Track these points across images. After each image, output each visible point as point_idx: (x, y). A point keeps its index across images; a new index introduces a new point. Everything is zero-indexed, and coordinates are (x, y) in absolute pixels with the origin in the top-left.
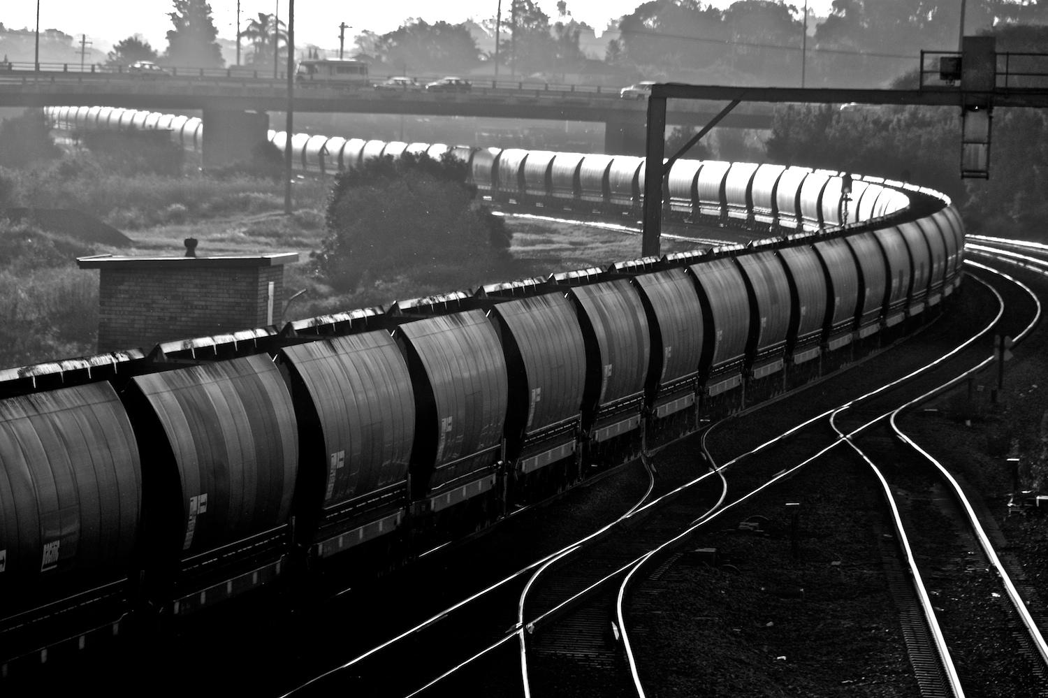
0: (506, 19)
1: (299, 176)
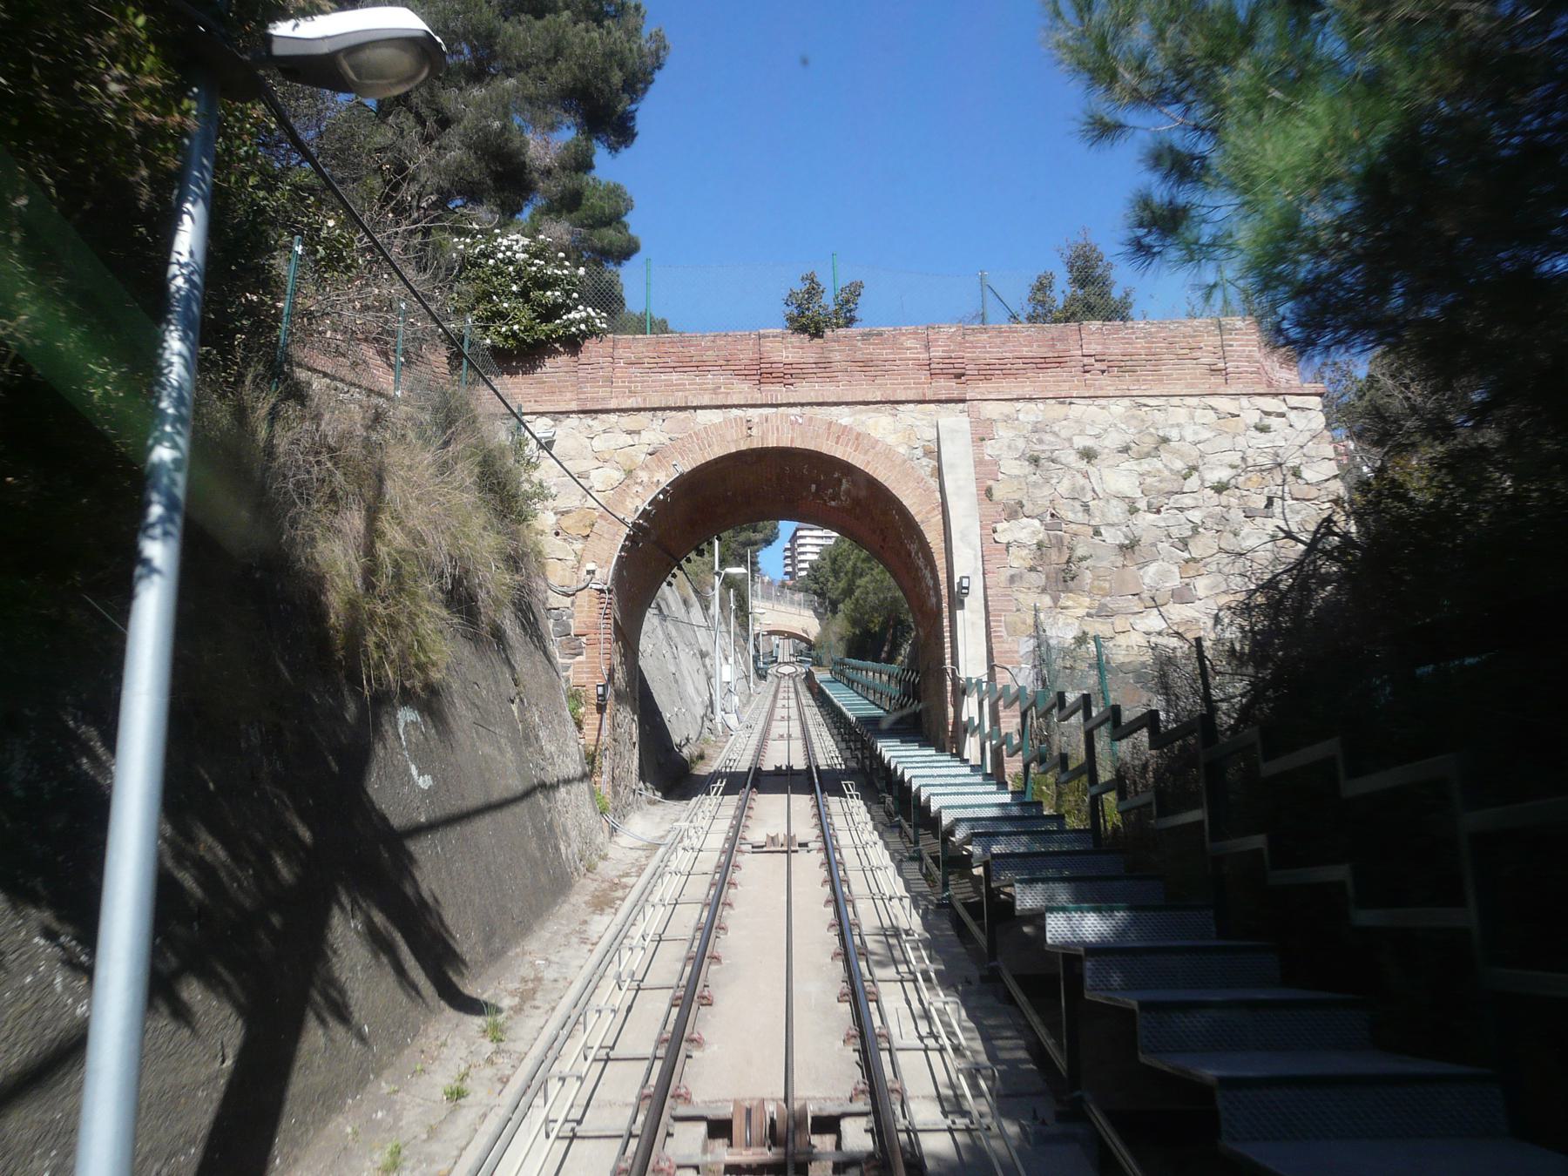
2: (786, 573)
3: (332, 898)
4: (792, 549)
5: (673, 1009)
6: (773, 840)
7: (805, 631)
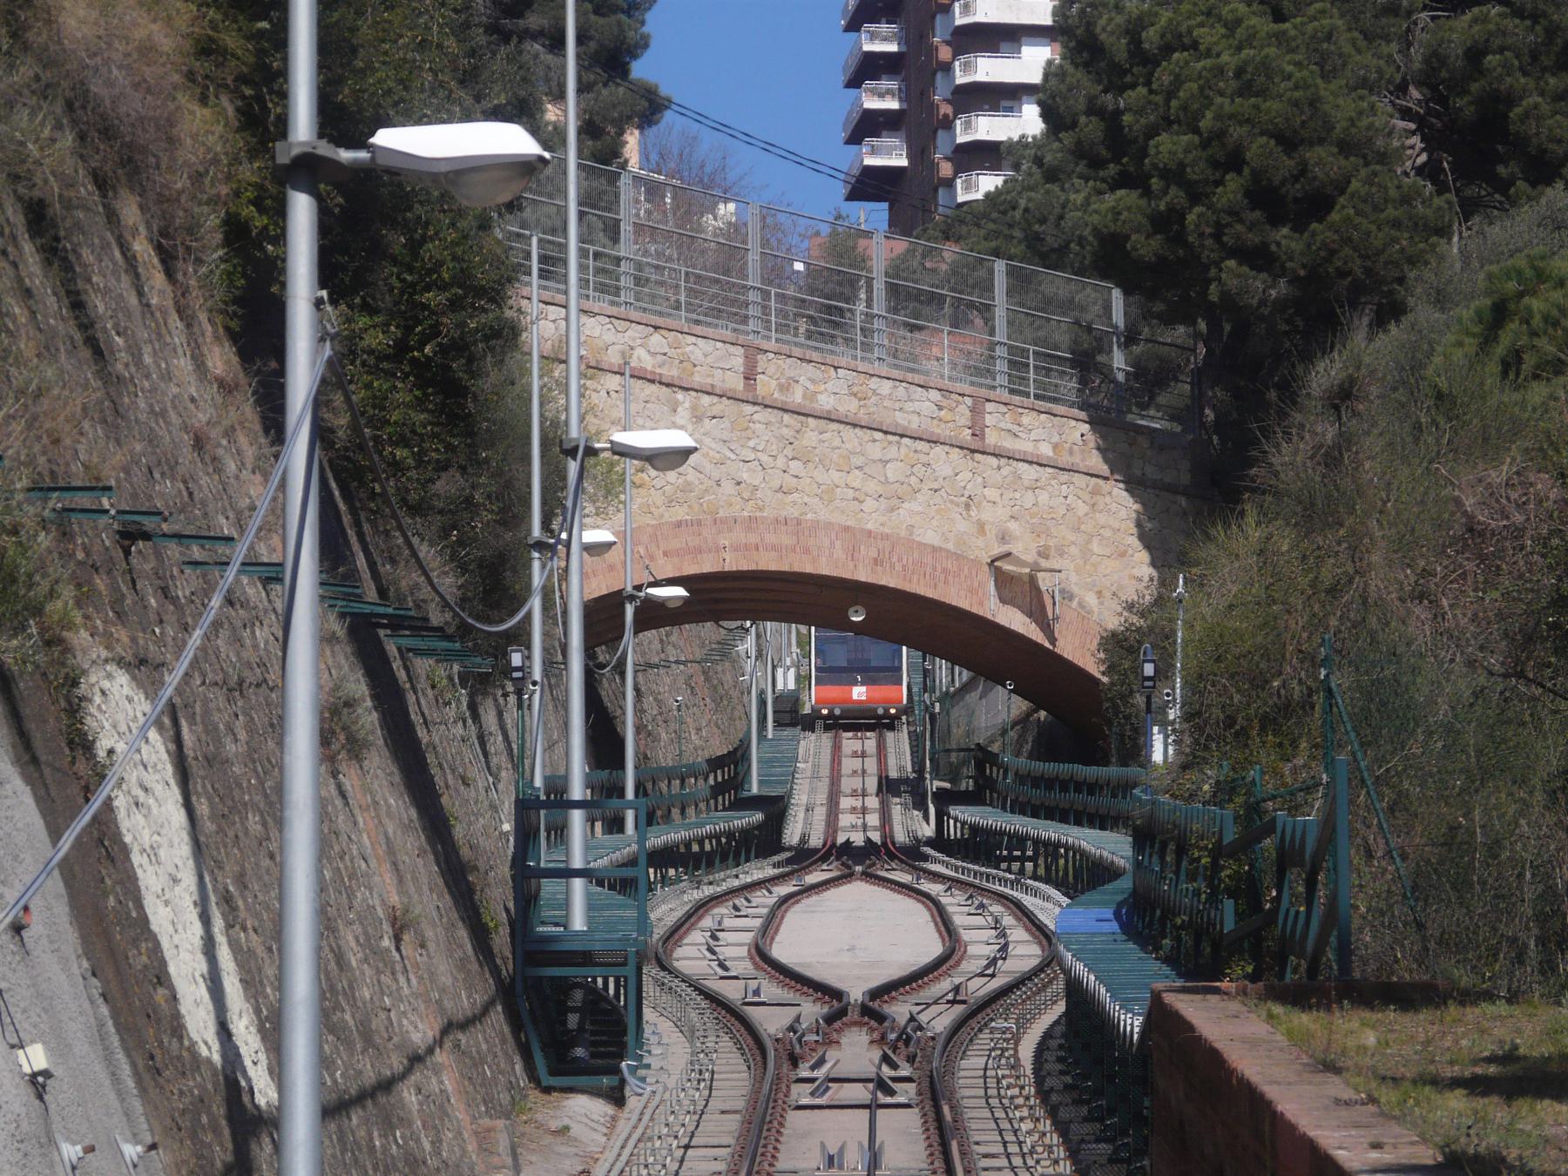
0: (195, 904)
1: (679, 591)
2: (870, 185)
5: (992, 438)
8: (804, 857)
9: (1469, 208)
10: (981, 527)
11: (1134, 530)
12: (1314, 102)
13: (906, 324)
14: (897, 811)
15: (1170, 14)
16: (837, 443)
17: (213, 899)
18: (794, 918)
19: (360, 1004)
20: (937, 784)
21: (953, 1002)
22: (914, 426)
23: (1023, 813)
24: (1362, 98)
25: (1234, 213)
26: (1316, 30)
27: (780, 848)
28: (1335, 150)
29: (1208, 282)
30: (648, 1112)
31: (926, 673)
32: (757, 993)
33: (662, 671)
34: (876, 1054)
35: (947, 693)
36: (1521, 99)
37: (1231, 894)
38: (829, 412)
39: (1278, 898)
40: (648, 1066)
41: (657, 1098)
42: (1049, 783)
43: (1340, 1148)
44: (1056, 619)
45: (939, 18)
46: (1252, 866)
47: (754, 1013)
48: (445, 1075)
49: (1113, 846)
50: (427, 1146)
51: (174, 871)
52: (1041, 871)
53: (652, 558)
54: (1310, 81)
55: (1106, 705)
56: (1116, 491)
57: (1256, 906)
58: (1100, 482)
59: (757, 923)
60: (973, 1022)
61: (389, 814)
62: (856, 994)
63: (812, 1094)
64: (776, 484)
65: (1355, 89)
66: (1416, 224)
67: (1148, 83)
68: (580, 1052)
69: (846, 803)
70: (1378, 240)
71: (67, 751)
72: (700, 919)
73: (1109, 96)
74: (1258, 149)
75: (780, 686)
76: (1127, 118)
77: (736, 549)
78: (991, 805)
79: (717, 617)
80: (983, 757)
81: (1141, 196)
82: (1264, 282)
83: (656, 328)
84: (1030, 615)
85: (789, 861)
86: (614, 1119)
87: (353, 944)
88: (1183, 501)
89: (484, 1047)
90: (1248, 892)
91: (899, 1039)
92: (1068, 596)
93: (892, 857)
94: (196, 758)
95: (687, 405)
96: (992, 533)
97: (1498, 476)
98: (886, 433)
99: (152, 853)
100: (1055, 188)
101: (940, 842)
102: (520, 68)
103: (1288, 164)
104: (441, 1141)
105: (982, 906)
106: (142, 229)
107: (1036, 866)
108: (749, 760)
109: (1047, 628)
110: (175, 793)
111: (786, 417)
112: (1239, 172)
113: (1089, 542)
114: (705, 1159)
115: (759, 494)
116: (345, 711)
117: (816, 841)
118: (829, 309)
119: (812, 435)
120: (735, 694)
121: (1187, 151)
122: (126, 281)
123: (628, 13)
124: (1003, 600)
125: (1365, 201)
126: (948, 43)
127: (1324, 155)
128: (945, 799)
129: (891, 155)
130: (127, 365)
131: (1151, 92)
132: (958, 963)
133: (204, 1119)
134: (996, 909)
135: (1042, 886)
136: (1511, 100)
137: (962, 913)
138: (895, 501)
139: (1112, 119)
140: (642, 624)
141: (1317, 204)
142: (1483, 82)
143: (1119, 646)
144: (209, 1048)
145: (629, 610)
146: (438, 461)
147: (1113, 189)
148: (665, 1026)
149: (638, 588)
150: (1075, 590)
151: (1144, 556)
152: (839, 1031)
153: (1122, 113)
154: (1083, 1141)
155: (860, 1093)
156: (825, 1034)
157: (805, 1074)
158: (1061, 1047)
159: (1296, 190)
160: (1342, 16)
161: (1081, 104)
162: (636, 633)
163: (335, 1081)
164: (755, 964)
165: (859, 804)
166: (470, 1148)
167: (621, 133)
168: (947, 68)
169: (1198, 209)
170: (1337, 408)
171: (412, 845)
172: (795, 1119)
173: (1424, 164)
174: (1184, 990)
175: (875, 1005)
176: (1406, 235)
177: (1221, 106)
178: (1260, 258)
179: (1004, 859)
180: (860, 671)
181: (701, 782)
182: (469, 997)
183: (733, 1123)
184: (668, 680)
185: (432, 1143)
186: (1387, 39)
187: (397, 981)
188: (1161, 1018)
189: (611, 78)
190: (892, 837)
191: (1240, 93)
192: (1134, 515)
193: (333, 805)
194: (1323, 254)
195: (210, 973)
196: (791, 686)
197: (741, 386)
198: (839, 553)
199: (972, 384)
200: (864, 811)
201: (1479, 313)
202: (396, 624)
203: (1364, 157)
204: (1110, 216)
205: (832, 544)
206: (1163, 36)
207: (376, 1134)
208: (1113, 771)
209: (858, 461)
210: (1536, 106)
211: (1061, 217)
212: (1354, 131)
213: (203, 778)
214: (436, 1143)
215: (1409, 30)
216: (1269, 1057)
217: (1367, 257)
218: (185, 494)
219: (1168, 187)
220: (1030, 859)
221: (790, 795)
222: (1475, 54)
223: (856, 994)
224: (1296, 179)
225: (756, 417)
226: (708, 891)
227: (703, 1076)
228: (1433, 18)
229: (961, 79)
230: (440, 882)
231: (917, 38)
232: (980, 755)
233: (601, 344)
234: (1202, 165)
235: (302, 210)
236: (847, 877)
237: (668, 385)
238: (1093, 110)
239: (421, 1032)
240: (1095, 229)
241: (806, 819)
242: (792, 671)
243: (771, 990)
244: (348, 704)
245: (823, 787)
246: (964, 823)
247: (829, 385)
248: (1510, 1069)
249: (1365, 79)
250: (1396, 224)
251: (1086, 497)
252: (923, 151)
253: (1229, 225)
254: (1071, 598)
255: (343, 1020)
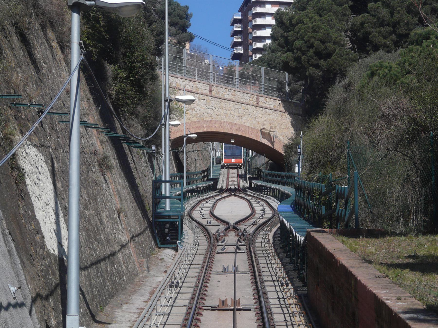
0: (54, 210)
1: (195, 135)
2: (236, 57)
3: (270, 159)
4: (244, 21)
5: (261, 104)
6: (223, 303)
7: (267, 135)
8: (222, 191)
9: (360, 57)
10: (258, 122)
11: (291, 123)
12: (328, 34)
13: (243, 83)
14: (241, 181)
15: (298, 16)
16: (229, 105)
17: (60, 208)
18: (219, 204)
19: (106, 233)
20: (249, 176)
21: (254, 225)
22: (245, 101)
23: (267, 182)
24: (338, 33)
25: (312, 57)
26: (328, 19)
27: (217, 189)
28: (332, 44)
29: (306, 72)
30: (183, 254)
31: (247, 153)
32: (210, 223)
33: (192, 152)
34: (236, 238)
35: (251, 157)
36: (372, 33)
37: (324, 204)
38: (227, 98)
39: (336, 206)
40: (184, 242)
41: (185, 250)
42: (272, 176)
43: (387, 299)
44: (274, 142)
45: (249, 23)
46: (329, 198)
47: (209, 228)
48: (131, 249)
49: (288, 190)
50: (124, 268)
51: (47, 202)
52: (271, 194)
53: (190, 129)
54: (328, 29)
55: (284, 159)
56: (287, 115)
57: (330, 208)
58: (283, 113)
59: (211, 205)
60: (258, 230)
61: (119, 184)
62: (232, 223)
63: (221, 250)
64: (216, 113)
65: (337, 31)
66: (350, 59)
67: (293, 30)
68: (168, 238)
69: (230, 180)
70: (342, 62)
71: (10, 169)
72: (199, 205)
73: (285, 33)
74: (317, 43)
75: (217, 156)
76: (289, 38)
77: (207, 127)
78: (260, 180)
79: (204, 141)
80: (259, 170)
81: (292, 54)
82: (318, 71)
83: (191, 81)
84: (269, 141)
85: (218, 192)
86: (175, 255)
87: (105, 217)
88: (300, 117)
89: (143, 240)
90: (328, 204)
91: (242, 235)
92: (276, 137)
93: (240, 191)
94: (58, 171)
95: (197, 97)
96: (261, 124)
97: (389, 102)
98: (239, 103)
99: (39, 198)
100: (274, 54)
101: (250, 188)
102: (161, 24)
103: (323, 47)
104: (128, 266)
105: (259, 202)
106: (55, 40)
107: (270, 193)
108: (210, 171)
109: (272, 144)
110: (50, 180)
111: (218, 99)
112: (313, 48)
113: (281, 126)
114: (195, 268)
115: (212, 115)
116: (106, 159)
117: (224, 187)
118: (227, 80)
119: (223, 103)
120: (208, 157)
121: (302, 44)
122: (48, 52)
123: (186, 19)
124: (263, 138)
125: (339, 54)
126: (251, 28)
127: (330, 44)
128: (250, 179)
129: (240, 50)
130: (46, 71)
131: (294, 32)
132: (254, 215)
133: (50, 271)
134: (262, 202)
135: (272, 198)
136: (370, 33)
137: (255, 204)
138: (241, 117)
139: (286, 38)
140: (188, 143)
141: (329, 55)
142: (364, 30)
143: (287, 147)
144: (54, 251)
145: (185, 139)
146: (136, 103)
147: (286, 53)
148: (189, 231)
149: (187, 135)
150: (278, 135)
151: (292, 129)
152: (228, 232)
153: (288, 37)
154: (286, 264)
155: (232, 249)
156: (225, 233)
157: (220, 244)
158: (279, 237)
159: (324, 52)
160: (334, 16)
161: (279, 35)
162: (186, 145)
163: (96, 254)
164: (210, 215)
165: (233, 180)
166: (137, 266)
167: (185, 44)
168: (251, 33)
169: (304, 56)
170: (346, 88)
171: (126, 192)
172: (217, 256)
173: (351, 47)
174: (316, 231)
175: (236, 226)
176: (348, 62)
177: (309, 35)
178: (317, 66)
179: (263, 191)
180: (233, 156)
181: (200, 175)
182: (139, 228)
183: (184, 310)
184: (194, 154)
185: (126, 267)
186: (344, 21)
187: (118, 226)
188: (308, 237)
189: (183, 32)
190: (240, 187)
191: (313, 32)
192: (290, 120)
193: (102, 182)
194: (330, 65)
195: (57, 229)
196: (219, 156)
197: (209, 93)
198: (229, 128)
199: (257, 93)
200: (234, 181)
201: (367, 74)
202: (128, 140)
203: (339, 45)
204: (285, 58)
205: (228, 126)
206: (297, 21)
207: (109, 267)
208: (286, 173)
209: (233, 109)
210: (375, 35)
211: (275, 60)
212: (336, 40)
213: (60, 176)
214: (127, 267)
215: (348, 19)
216: (347, 257)
217: (340, 66)
218: (62, 104)
219: (298, 52)
220: (269, 191)
221: (219, 178)
222: (362, 24)
223: (232, 223)
224: (324, 50)
225: (212, 99)
226: (201, 198)
227: (197, 244)
228: (353, 17)
229: (254, 35)
230: (134, 200)
231: (245, 27)
232: (258, 170)
233: (179, 84)
234: (305, 47)
235: (76, 18)
236: (231, 195)
237: (193, 93)
238: (282, 36)
239: (124, 238)
240: (282, 60)
241: (222, 183)
242: (220, 153)
243: (213, 222)
244: (106, 158)
245: (226, 176)
246: (255, 184)
247: (227, 93)
248: (417, 261)
249: (339, 29)
250: (346, 59)
251: (280, 116)
252: (246, 49)
253: (310, 59)
254: (277, 137)
255: (101, 237)
